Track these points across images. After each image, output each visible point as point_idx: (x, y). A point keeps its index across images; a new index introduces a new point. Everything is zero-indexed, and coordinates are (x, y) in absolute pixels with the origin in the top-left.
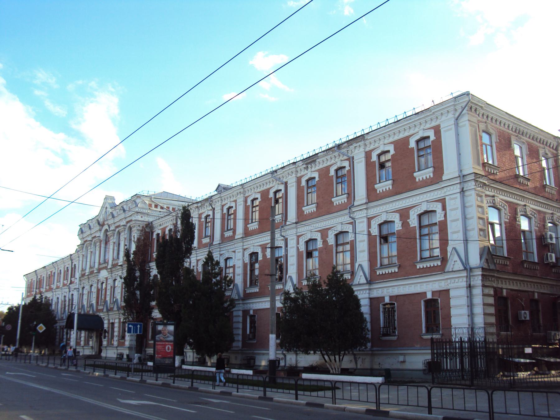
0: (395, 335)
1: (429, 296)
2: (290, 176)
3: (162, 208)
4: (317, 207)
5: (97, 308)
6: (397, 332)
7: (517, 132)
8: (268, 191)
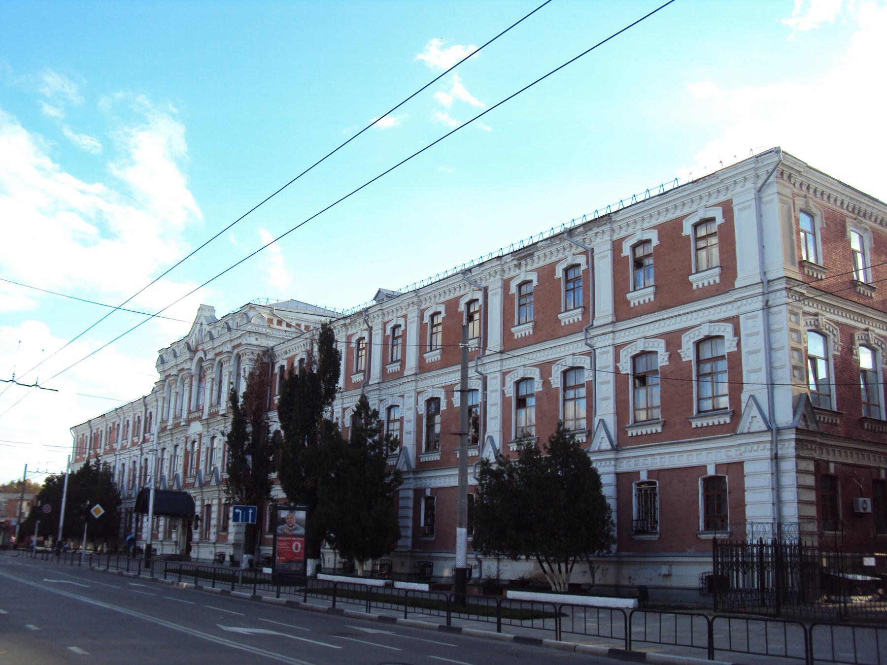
0: (656, 533)
1: (711, 471)
2: (492, 279)
3: (289, 325)
4: (534, 328)
5: (184, 481)
6: (658, 528)
7: (856, 212)
8: (457, 300)
